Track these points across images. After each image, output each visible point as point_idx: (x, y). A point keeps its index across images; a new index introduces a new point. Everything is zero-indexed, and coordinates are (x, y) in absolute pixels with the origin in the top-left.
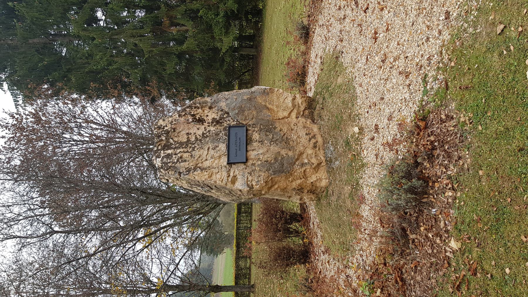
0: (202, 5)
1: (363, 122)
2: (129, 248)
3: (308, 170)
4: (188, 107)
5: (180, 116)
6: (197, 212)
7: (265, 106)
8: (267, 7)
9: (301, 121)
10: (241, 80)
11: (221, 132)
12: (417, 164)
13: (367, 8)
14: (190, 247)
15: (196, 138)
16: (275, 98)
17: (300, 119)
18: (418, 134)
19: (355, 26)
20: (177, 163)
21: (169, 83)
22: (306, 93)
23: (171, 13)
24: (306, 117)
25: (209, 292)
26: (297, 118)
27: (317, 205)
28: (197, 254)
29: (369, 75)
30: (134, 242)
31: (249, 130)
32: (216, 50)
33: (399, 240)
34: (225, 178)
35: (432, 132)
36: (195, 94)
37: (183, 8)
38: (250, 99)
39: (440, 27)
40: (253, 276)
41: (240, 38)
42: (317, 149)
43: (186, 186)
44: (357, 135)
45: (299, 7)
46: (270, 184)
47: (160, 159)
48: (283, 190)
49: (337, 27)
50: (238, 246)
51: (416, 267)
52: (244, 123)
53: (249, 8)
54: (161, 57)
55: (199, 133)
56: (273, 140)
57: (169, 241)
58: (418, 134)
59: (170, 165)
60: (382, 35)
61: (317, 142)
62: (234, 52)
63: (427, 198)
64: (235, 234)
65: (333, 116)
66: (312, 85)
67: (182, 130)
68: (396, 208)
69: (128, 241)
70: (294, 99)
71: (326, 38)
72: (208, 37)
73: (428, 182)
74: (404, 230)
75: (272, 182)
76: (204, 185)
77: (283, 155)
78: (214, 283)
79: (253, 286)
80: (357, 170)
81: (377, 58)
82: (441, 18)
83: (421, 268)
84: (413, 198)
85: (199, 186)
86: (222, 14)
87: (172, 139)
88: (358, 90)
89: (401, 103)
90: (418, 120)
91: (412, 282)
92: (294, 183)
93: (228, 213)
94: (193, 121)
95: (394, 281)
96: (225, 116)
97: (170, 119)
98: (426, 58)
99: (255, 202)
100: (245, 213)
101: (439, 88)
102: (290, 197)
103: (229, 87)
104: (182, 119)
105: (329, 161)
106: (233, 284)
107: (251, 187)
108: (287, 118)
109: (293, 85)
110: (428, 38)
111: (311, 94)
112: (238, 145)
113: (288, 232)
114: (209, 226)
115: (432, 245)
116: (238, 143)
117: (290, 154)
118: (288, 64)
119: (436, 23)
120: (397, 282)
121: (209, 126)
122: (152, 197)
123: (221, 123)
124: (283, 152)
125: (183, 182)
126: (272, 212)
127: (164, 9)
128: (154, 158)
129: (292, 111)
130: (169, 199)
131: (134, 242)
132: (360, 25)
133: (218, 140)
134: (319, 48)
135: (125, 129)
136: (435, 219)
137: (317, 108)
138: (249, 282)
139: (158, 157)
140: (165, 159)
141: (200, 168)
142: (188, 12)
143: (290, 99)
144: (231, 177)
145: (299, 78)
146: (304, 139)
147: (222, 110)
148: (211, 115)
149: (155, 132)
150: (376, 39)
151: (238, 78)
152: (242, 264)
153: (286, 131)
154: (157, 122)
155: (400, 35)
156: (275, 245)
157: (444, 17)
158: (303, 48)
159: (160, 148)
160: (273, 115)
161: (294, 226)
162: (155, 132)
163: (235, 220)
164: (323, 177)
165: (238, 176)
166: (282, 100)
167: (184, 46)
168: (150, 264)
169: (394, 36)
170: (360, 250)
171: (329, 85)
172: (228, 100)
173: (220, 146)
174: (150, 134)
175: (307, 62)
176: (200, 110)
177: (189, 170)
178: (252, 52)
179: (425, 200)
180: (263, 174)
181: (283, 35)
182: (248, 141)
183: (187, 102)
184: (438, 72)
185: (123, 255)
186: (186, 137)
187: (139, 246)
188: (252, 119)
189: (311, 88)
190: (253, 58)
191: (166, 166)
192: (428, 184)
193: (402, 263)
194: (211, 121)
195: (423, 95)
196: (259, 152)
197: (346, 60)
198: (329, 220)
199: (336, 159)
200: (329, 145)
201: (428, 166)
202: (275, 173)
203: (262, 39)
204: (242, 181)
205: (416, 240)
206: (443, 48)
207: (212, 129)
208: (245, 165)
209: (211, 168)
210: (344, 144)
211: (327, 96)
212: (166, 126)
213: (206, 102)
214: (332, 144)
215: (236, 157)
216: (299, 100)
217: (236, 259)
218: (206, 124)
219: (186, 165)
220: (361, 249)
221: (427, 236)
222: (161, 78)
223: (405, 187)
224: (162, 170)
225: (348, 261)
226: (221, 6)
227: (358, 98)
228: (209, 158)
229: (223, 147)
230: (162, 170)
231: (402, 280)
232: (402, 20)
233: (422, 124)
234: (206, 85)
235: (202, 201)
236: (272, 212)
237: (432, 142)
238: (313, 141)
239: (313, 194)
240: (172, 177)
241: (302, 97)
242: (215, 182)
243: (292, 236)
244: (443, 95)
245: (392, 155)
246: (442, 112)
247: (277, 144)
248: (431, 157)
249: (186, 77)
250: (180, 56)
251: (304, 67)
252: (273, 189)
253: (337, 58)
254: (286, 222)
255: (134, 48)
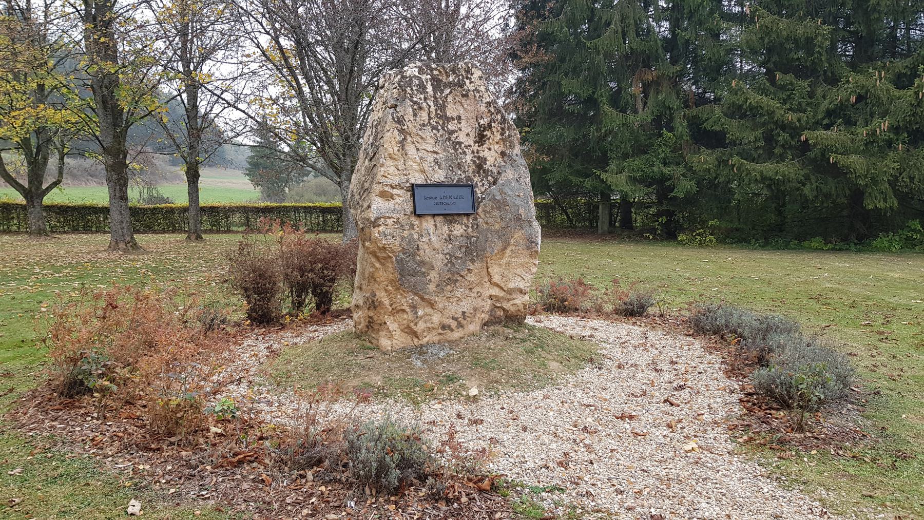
0: (681, 136)
1: (486, 401)
2: (261, 24)
3: (405, 316)
4: (503, 116)
5: (489, 104)
6: (324, 139)
7: (509, 245)
8: (680, 249)
9: (485, 304)
10: (553, 208)
11: (464, 172)
12: (422, 478)
13: (672, 404)
14: (263, 128)
15: (453, 132)
16: (522, 260)
17: (489, 301)
18: (470, 480)
19: (644, 387)
20: (412, 101)
21: (544, 83)
22: (533, 314)
23: (665, 85)
24: (491, 311)
25: (187, 163)
26: (491, 297)
27: (349, 334)
28: (249, 140)
29: (563, 410)
30: (271, 32)
31: (468, 219)
32: (603, 162)
33: (302, 454)
34: (389, 181)
35: (474, 499)
36: (527, 129)
37: (675, 103)
38: (518, 218)
39: (639, 509)
40: (215, 237)
41: (626, 205)
42: (440, 331)
43: (373, 117)
44: (464, 393)
45: (679, 300)
46: (380, 254)
47: (417, 74)
48: (372, 277)
49: (643, 359)
50: (266, 210)
51: (263, 481)
52: (480, 210)
53: (679, 216)
54: (589, 69)
55: (461, 136)
56: (453, 259)
57: (274, 91)
58: (470, 480)
59: (408, 89)
60: (628, 426)
61: (452, 330)
62: (602, 194)
63: (372, 494)
64: (287, 204)
65: (495, 355)
66: (547, 324)
67: (465, 109)
68: (353, 448)
69: (272, 22)
70: (521, 291)
71: (625, 343)
72: (625, 148)
73: (397, 495)
74: (319, 462)
75: (384, 258)
76: (376, 147)
77: (428, 274)
78: (203, 172)
79: (199, 237)
80: (408, 394)
81: (589, 419)
82: (652, 510)
83: (261, 490)
84: (370, 470)
85: (375, 139)
86: (666, 171)
87: (451, 92)
88: (539, 394)
89: (517, 456)
90: (493, 479)
91: (239, 477)
92: (383, 294)
93: (322, 192)
94: (480, 126)
95: (237, 450)
96: (490, 178)
97: (483, 89)
98: (591, 490)
99: (344, 236)
100: (324, 221)
101: (543, 509)
102: (361, 289)
103: (539, 185)
104: (483, 108)
105: (420, 350)
106: (202, 204)
107: (375, 224)
108: (490, 281)
109: (546, 292)
110: (621, 492)
111: (530, 320)
112: (443, 201)
113: (300, 289)
114: (300, 159)
115: (299, 504)
116: (446, 201)
117: (432, 287)
118: (581, 283)
119: (646, 504)
120: (236, 454)
121: (473, 152)
122: (348, 60)
123: (479, 172)
124: (433, 275)
125: (381, 112)
126: (332, 263)
127: (671, 71)
128: (419, 64)
129: (502, 288)
130: (347, 89)
131: (271, 32)
132: (644, 394)
133: (450, 168)
134: (608, 333)
135: (463, 10)
136: (339, 507)
137: (507, 331)
138: (205, 232)
139: (421, 70)
140: (417, 82)
141: (405, 139)
142: (668, 112)
143: (522, 285)
144: (390, 190)
145: (557, 303)
146: (455, 309)
147: (499, 173)
148: (491, 155)
149: (461, 64)
150: (622, 418)
151: (556, 200)
152: (236, 218)
153: (468, 278)
154: (477, 67)
155: (628, 453)
156: (278, 269)
157: (654, 513)
158: (608, 308)
159: (435, 72)
160: (494, 258)
161: (310, 301)
162: (461, 64)
163: (310, 204)
164: (394, 341)
165: (392, 202)
166: (518, 271)
167: (607, 109)
168: (235, 60)
169: (626, 444)
170: (279, 402)
171: (546, 348)
172: (517, 182)
173: (440, 171)
174: (456, 52)
175: (585, 314)
176: (499, 137)
177: (400, 121)
178: (603, 225)
179: (368, 491)
180: (397, 243)
181: (632, 275)
182: (450, 218)
183: (513, 116)
184: (567, 507)
185: (248, 14)
186: (455, 115)
187: (264, 40)
188: (487, 223)
189: (540, 322)
190: (592, 227)
191: (405, 83)
192: (392, 495)
193: (267, 461)
194: (481, 155)
195: (531, 488)
196: (433, 236)
197: (588, 373)
198: (325, 354)
199: (424, 362)
200: (447, 350)
201: (421, 494)
202: (400, 262)
203: (625, 241)
204: (385, 208)
205: (304, 481)
206: (606, 514)
207: (467, 157)
208: (411, 213)
209: (404, 157)
210: (450, 373)
211: (528, 345)
212: (471, 82)
213: (512, 147)
214: (448, 355)
215: (424, 199)
216: (520, 300)
217: (245, 207)
218: (476, 147)
219: (409, 116)
220: (281, 404)
221: (311, 495)
222: (551, 68)
223: (388, 459)
224: (399, 77)
225: (260, 385)
226: (681, 169)
227: (526, 393)
228: (420, 154)
229: (439, 176)
230: (399, 77)
231: (240, 462)
232: (651, 455)
233: (486, 484)
234: (543, 149)
235: (344, 146)
236: (332, 263)
237: (458, 499)
238: (454, 324)
239: (367, 327)
240: (388, 94)
241: (525, 305)
242: (382, 165)
243: (294, 295)
244: (533, 514)
245: (436, 444)
246: (505, 514)
247: (446, 265)
248: (435, 497)
249: (555, 113)
250: (591, 102)
251: (577, 309)
252: (373, 260)
253: (591, 361)
254: (316, 287)
255: (603, 21)
